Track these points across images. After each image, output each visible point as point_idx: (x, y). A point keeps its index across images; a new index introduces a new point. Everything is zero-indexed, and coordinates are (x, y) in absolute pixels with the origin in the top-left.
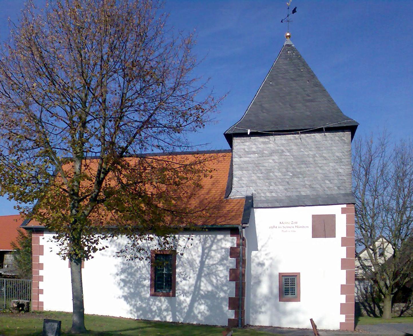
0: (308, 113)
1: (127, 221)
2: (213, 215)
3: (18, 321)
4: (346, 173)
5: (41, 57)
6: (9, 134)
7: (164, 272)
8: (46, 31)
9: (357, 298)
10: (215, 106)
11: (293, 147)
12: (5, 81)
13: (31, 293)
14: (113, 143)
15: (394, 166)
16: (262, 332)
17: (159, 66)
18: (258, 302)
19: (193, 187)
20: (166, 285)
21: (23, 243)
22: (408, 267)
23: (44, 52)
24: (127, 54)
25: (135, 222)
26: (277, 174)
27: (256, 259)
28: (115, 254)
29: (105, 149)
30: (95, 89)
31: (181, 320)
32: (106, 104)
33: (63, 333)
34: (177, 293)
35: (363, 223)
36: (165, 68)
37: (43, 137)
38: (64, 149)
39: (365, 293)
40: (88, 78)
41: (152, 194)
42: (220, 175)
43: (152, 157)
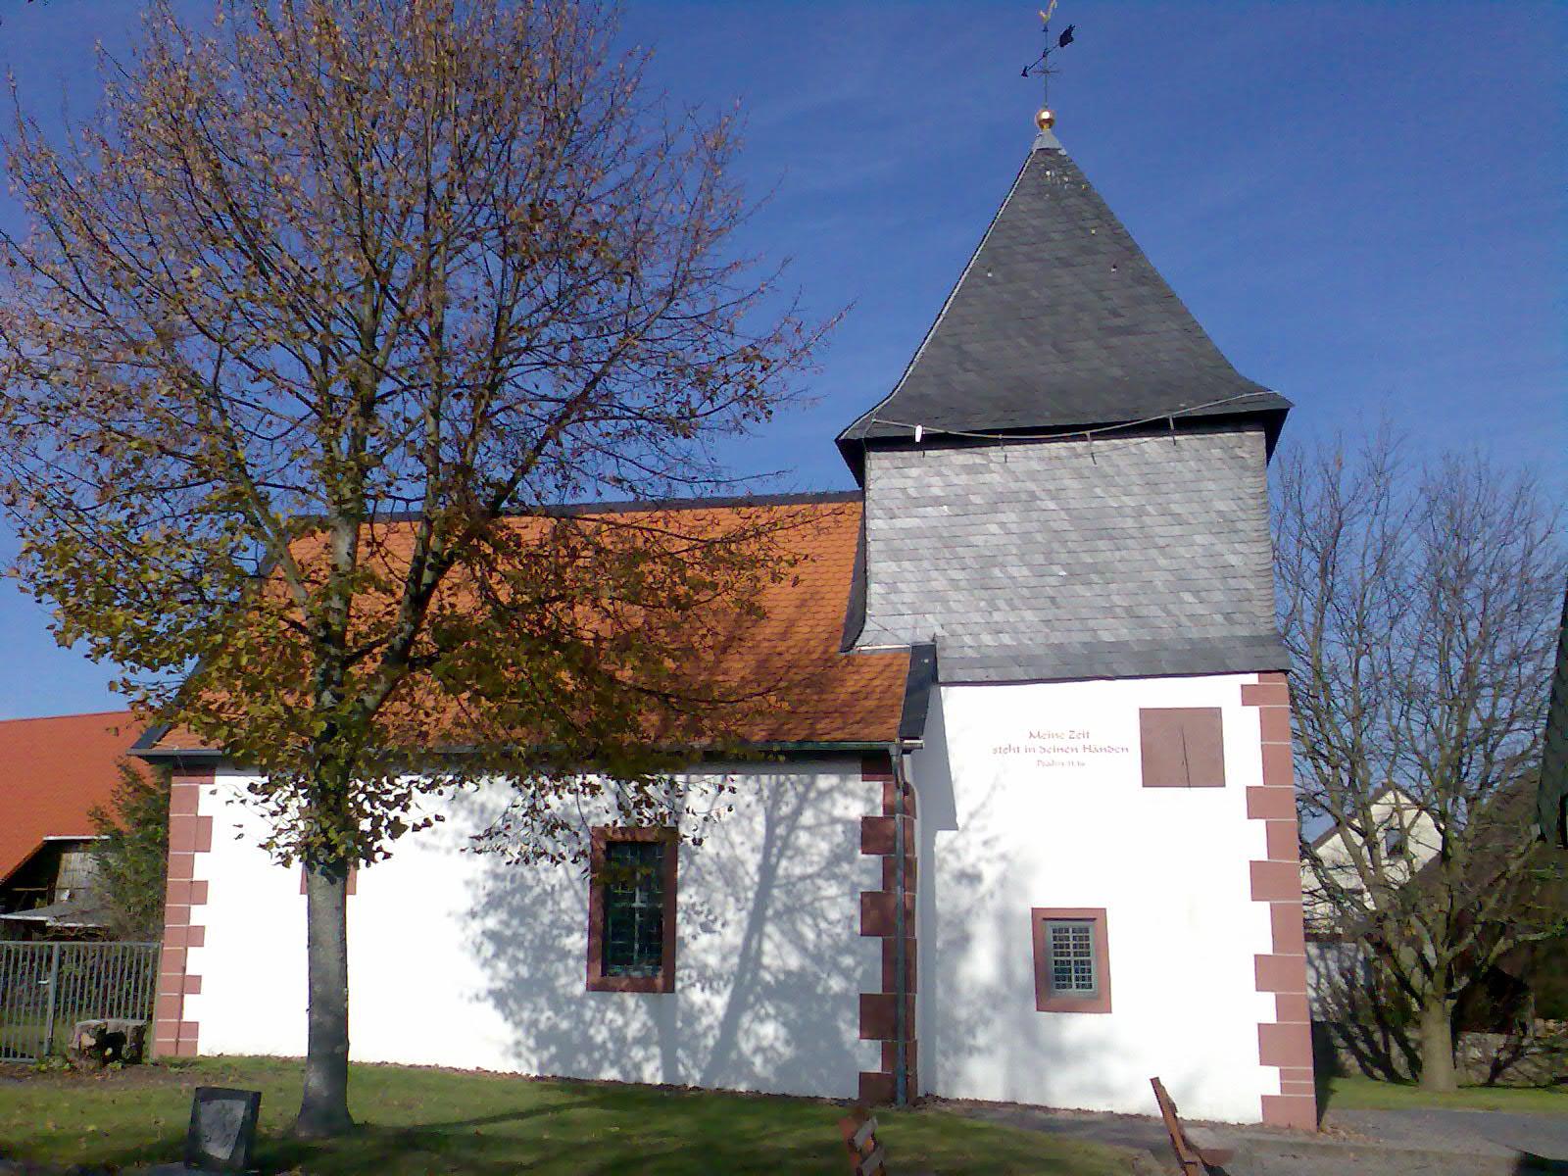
0: (1117, 372)
1: (512, 728)
2: (803, 709)
3: (92, 1101)
4: (1254, 568)
5: (219, 182)
6: (102, 433)
7: (637, 904)
8: (234, 95)
9: (1316, 1006)
10: (805, 349)
11: (1067, 482)
12: (86, 257)
13: (153, 989)
14: (466, 470)
15: (1423, 545)
16: (981, 1124)
17: (620, 219)
18: (962, 1013)
19: (733, 616)
20: (641, 951)
21: (137, 809)
22: (1502, 900)
23: (226, 164)
24: (512, 182)
25: (540, 733)
26: (1014, 571)
27: (950, 858)
28: (465, 842)
29: (440, 489)
30: (408, 291)
31: (695, 1078)
32: (445, 340)
33: (267, 1138)
34: (682, 980)
35: (1320, 737)
36: (642, 227)
37: (224, 447)
38: (297, 488)
39: (1345, 987)
40: (382, 255)
41: (597, 639)
42: (825, 576)
43: (597, 517)
